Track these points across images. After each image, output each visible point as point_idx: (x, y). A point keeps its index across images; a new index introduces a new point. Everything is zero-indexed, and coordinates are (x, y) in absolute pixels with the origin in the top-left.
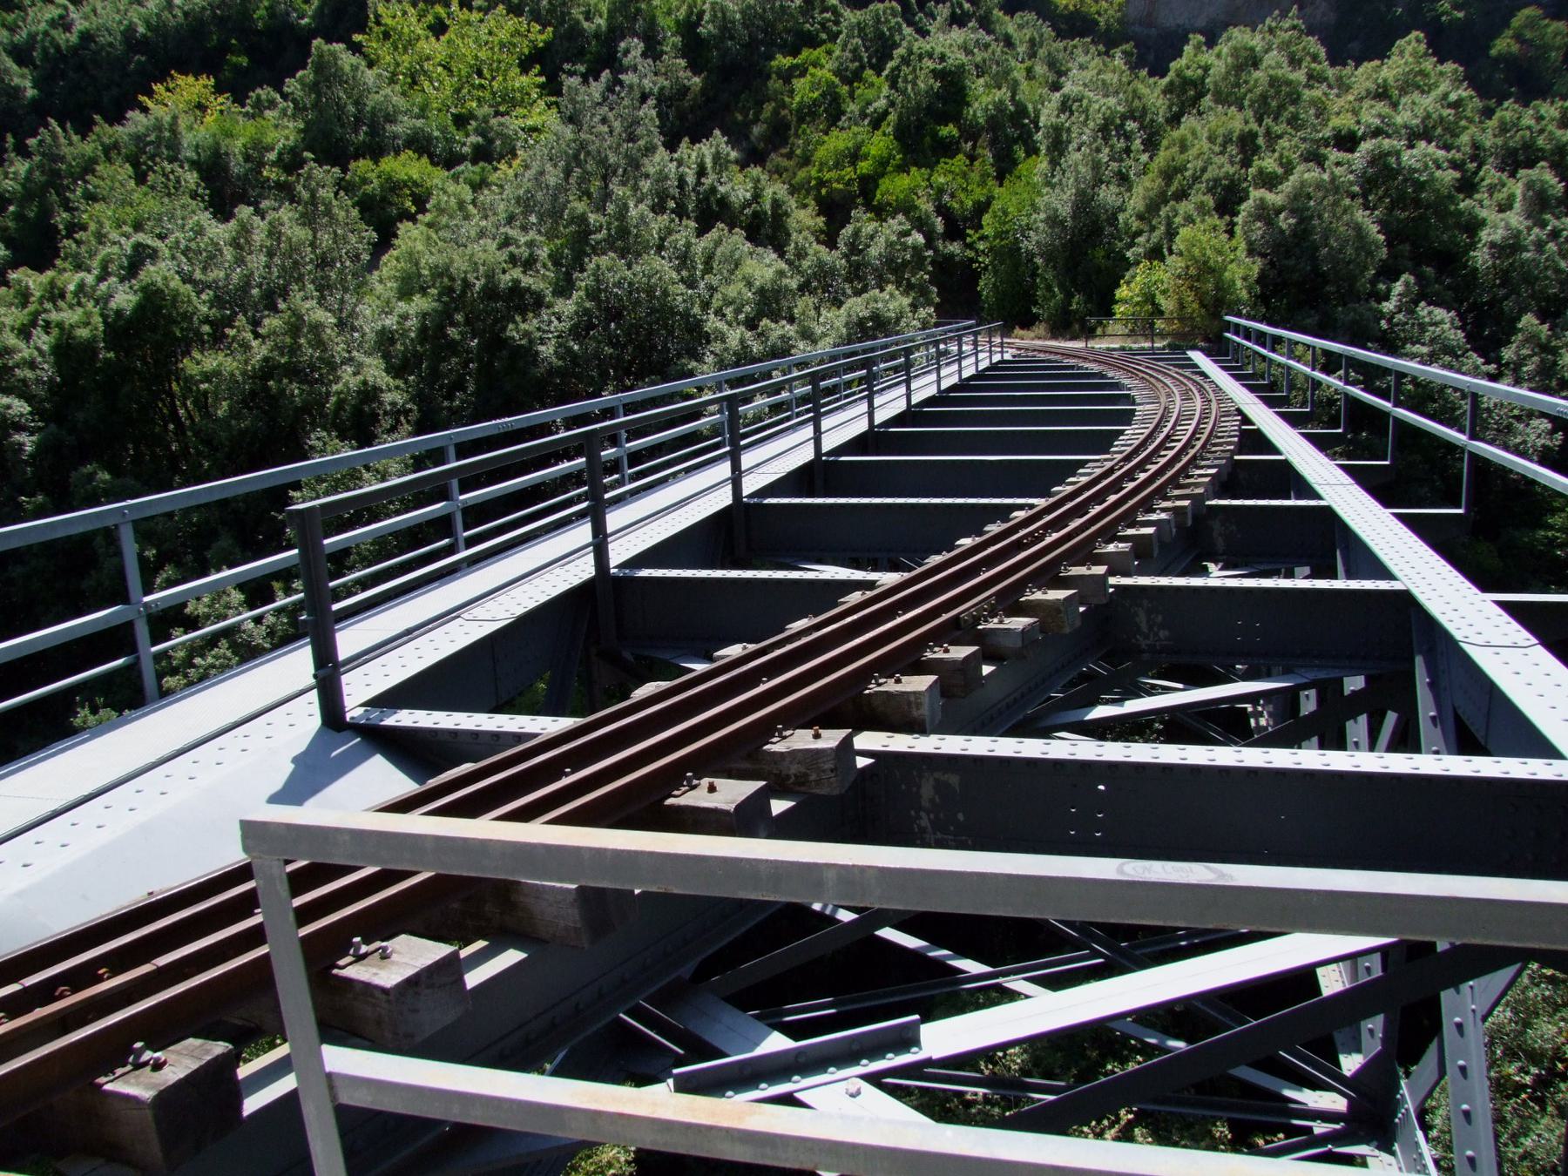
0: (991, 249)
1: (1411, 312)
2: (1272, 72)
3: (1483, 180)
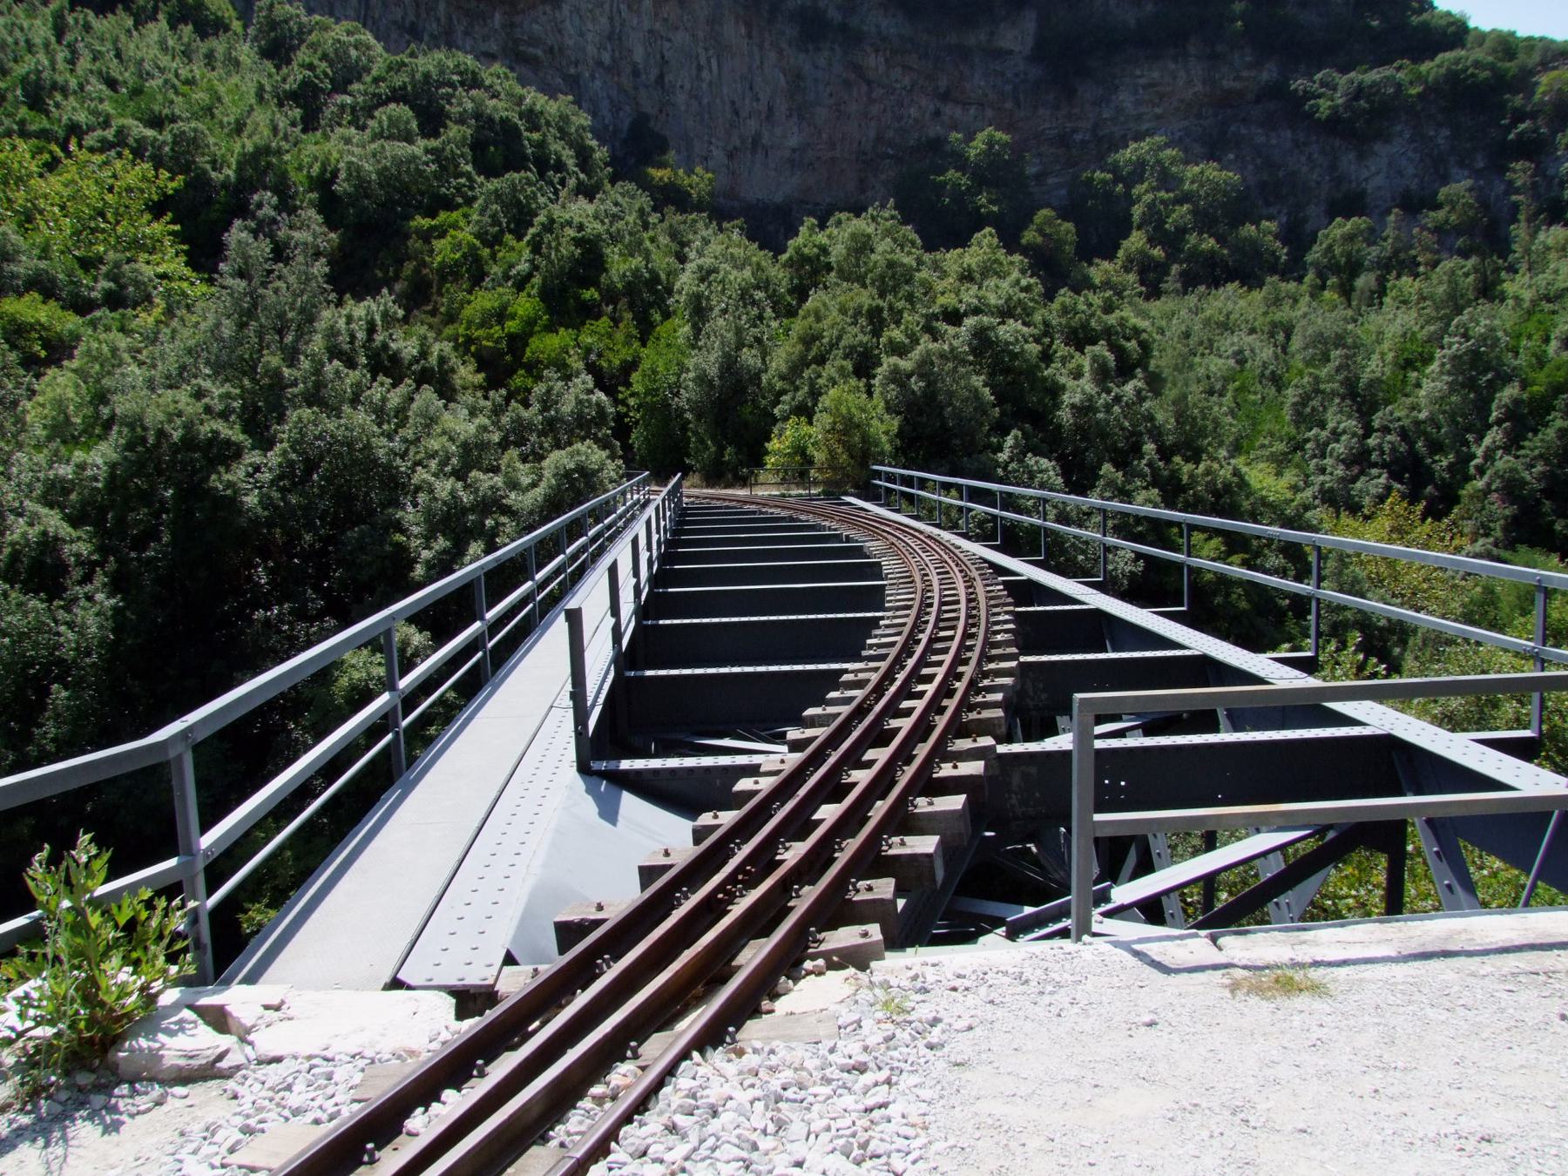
0: (640, 406)
1: (1021, 461)
2: (888, 257)
3: (1056, 352)
